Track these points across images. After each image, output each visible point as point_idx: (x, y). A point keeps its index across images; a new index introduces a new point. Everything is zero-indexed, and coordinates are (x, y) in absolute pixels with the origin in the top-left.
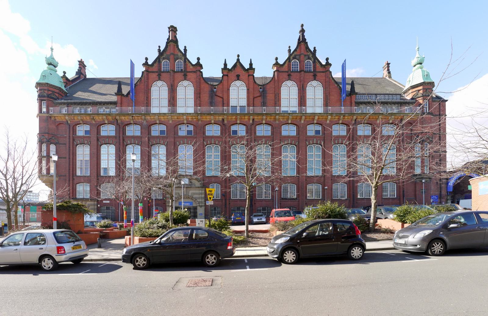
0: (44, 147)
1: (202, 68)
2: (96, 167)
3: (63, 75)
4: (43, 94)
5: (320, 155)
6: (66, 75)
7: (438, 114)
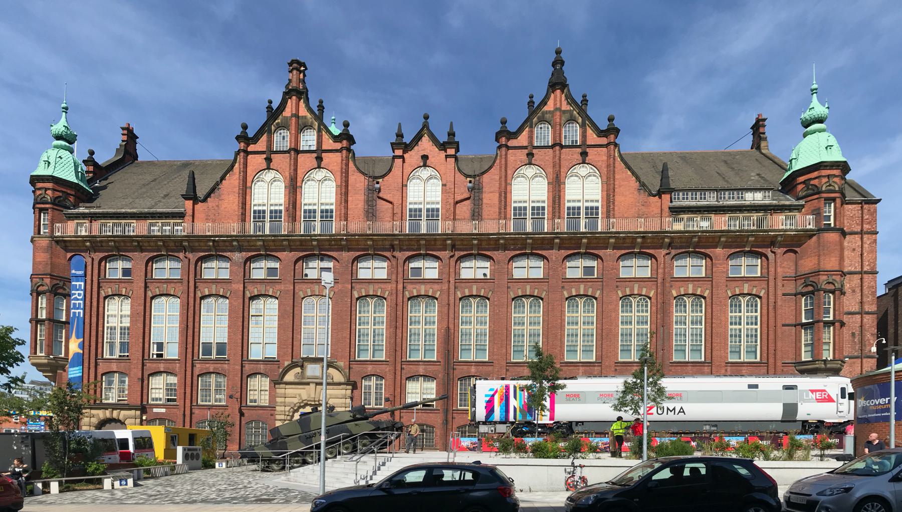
0: (43, 302)
1: (354, 143)
2: (141, 340)
4: (44, 197)
5: (756, 330)
7: (859, 230)
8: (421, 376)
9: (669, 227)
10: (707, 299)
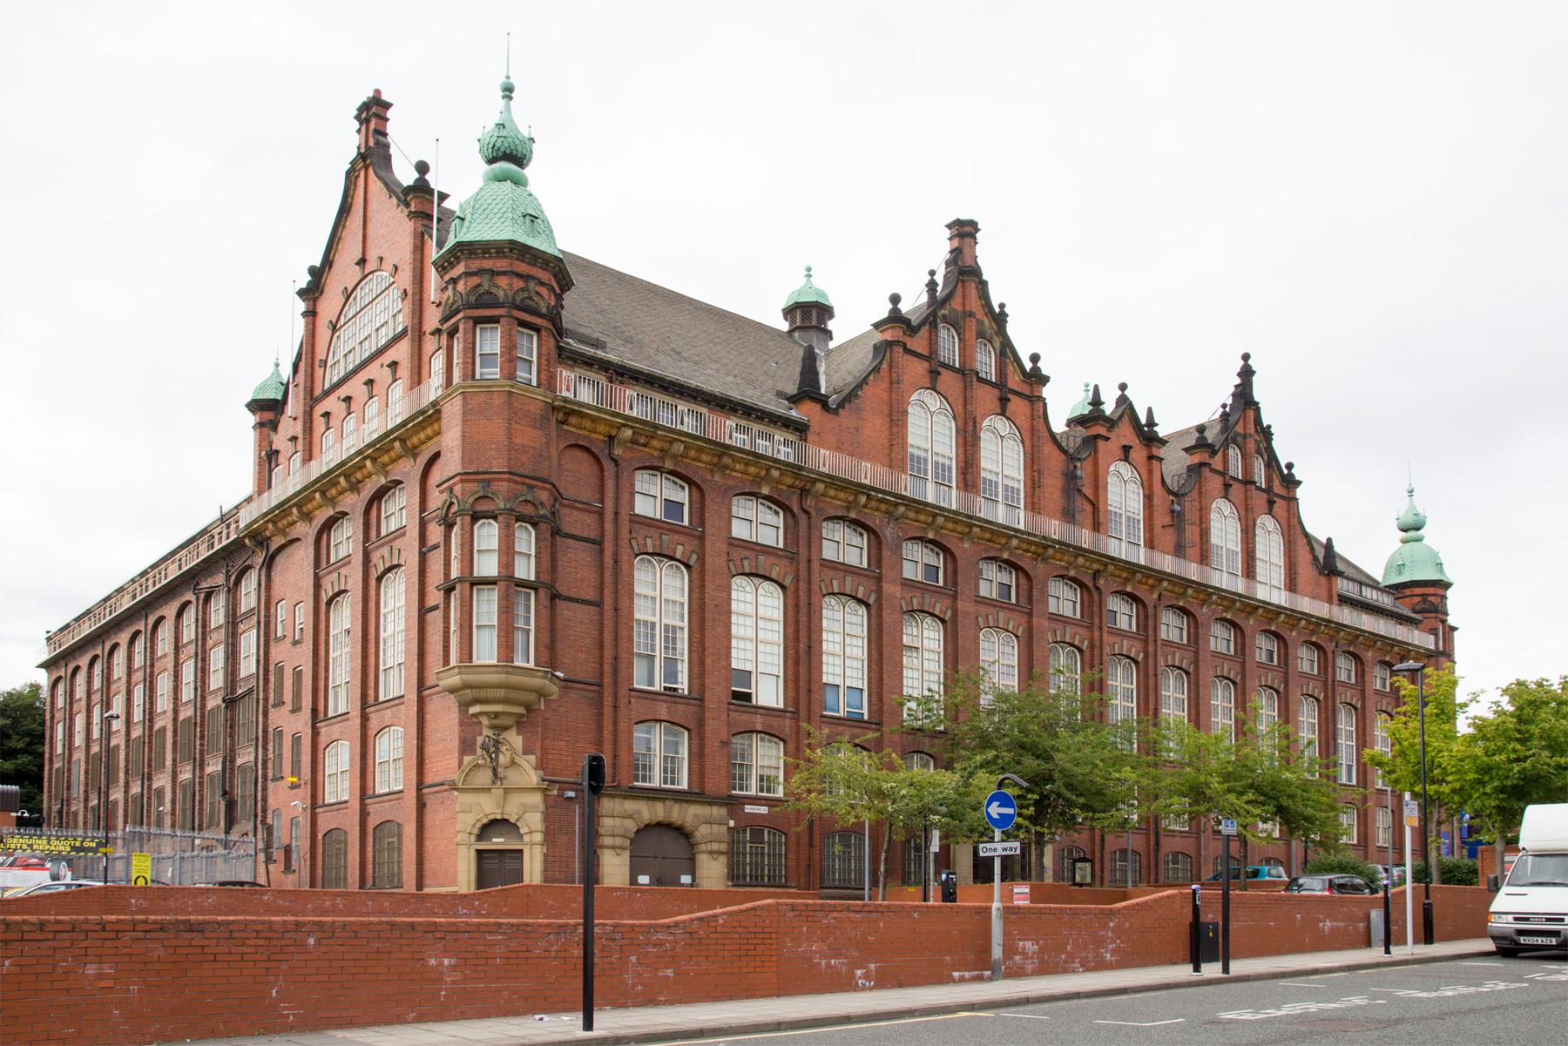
3: (416, 181)
6: (427, 177)
8: (758, 732)
9: (568, 390)
10: (789, 593)
